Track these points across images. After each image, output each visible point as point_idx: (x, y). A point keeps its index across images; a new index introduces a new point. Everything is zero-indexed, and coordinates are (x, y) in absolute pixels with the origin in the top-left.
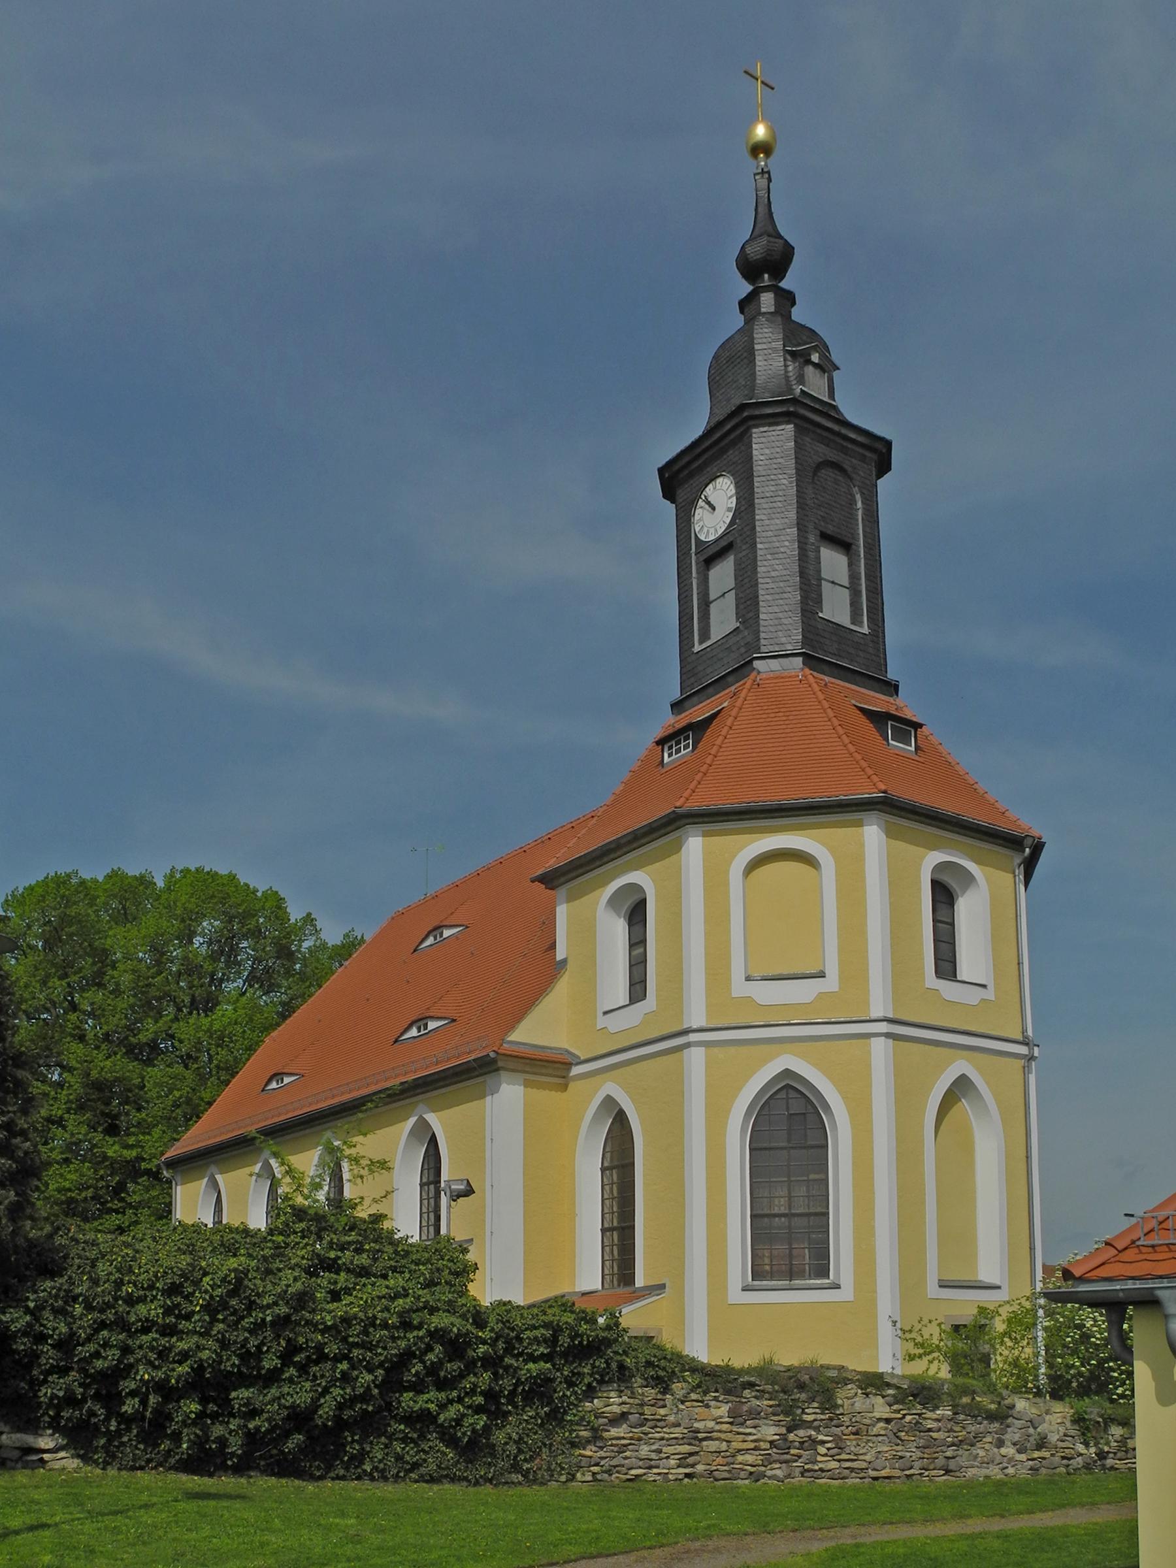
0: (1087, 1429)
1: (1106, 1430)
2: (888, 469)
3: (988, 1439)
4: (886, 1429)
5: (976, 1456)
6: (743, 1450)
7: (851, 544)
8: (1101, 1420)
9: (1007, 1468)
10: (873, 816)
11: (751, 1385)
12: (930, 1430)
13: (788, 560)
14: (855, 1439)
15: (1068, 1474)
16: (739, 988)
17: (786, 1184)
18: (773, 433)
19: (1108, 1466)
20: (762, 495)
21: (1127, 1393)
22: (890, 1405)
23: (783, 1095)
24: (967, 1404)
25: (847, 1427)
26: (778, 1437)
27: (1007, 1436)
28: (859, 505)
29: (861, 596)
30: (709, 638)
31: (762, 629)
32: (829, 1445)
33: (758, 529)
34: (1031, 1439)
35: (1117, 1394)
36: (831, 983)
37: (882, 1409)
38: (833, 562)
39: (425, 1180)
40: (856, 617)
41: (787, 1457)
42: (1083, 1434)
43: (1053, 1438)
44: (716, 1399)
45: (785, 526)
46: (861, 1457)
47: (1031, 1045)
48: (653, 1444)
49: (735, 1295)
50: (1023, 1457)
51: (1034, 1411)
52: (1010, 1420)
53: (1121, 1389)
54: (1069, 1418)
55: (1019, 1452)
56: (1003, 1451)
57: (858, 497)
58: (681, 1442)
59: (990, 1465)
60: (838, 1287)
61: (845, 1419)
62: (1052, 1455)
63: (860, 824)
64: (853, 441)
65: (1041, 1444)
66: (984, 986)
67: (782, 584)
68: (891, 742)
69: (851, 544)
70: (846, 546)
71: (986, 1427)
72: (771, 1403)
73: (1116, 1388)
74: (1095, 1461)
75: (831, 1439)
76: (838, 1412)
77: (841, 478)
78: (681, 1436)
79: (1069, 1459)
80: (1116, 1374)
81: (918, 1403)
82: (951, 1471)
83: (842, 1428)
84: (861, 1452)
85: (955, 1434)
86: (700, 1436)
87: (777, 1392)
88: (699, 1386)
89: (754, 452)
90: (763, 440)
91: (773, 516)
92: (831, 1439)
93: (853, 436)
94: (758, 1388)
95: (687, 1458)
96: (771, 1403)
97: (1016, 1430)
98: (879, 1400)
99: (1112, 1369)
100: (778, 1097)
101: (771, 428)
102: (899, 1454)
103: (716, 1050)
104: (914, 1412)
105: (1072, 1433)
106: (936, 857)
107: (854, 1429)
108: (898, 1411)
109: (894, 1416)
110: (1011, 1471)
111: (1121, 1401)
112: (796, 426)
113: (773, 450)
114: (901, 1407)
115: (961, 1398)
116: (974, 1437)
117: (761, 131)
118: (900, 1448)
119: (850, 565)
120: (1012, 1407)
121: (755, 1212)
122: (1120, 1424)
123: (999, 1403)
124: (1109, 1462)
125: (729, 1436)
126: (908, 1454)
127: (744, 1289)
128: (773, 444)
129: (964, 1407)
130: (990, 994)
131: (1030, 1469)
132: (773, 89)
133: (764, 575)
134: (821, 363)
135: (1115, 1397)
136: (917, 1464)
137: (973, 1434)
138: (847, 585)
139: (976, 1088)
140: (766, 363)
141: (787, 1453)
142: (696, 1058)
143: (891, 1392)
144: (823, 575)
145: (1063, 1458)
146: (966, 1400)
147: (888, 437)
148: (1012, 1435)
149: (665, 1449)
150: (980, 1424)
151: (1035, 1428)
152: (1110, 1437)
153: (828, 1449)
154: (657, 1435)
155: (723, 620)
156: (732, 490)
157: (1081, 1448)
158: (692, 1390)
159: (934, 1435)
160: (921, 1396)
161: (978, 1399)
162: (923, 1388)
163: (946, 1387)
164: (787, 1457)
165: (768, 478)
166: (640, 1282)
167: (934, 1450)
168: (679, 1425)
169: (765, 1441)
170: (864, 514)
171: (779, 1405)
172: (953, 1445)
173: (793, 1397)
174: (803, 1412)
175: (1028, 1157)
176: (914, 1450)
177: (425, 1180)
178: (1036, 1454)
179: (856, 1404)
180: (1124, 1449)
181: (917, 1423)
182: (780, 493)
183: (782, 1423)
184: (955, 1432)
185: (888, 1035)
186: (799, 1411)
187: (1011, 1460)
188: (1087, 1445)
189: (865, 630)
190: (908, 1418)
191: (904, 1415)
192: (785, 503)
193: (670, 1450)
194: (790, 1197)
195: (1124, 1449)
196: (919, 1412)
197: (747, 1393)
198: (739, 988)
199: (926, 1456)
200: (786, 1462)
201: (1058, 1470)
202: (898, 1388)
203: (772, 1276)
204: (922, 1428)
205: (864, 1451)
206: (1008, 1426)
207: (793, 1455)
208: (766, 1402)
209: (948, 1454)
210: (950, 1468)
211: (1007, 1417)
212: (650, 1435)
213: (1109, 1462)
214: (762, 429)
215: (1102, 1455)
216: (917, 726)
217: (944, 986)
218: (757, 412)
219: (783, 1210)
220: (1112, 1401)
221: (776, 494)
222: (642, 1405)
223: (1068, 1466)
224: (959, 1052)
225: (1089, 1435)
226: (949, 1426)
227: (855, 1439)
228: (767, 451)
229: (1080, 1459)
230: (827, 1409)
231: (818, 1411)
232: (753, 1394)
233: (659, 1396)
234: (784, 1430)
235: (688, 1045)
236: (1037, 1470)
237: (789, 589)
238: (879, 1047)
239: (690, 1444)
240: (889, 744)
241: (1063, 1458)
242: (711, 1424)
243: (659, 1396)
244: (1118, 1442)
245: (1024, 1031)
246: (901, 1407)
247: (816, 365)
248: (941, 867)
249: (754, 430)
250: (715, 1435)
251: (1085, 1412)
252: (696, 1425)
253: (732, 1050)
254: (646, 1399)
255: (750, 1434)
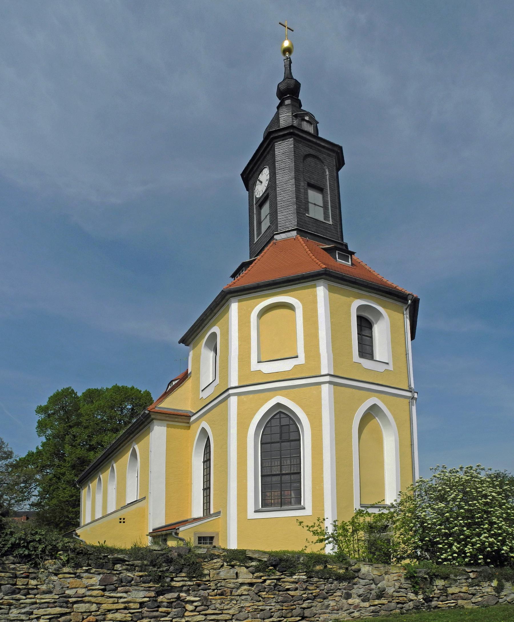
0: (416, 583)
1: (431, 583)
2: (343, 164)
3: (339, 593)
4: (249, 590)
5: (328, 606)
6: (113, 610)
7: (324, 189)
8: (427, 576)
9: (353, 612)
10: (322, 282)
11: (122, 561)
12: (288, 590)
13: (291, 193)
14: (220, 599)
15: (402, 613)
16: (255, 366)
17: (279, 459)
18: (284, 143)
19: (433, 606)
20: (279, 168)
21: (449, 557)
22: (253, 574)
23: (278, 416)
24: (321, 570)
25: (214, 590)
26: (147, 599)
27: (353, 591)
28: (327, 173)
29: (328, 210)
30: (261, 234)
31: (279, 223)
32: (195, 604)
33: (277, 182)
34: (373, 592)
35: (442, 559)
36: (301, 360)
37: (245, 576)
38: (314, 196)
39: (205, 487)
40: (326, 217)
41: (155, 614)
42: (414, 587)
43: (390, 591)
44: (87, 571)
45: (289, 179)
46: (225, 612)
47: (413, 392)
48: (24, 607)
49: (251, 514)
50: (367, 604)
51: (376, 572)
52: (356, 580)
53: (445, 555)
54: (403, 576)
55: (363, 601)
56: (350, 601)
57: (327, 170)
58: (52, 605)
59: (340, 611)
60: (304, 508)
61: (211, 584)
62: (389, 602)
63: (315, 286)
64: (324, 147)
65: (381, 595)
66: (387, 363)
67: (288, 203)
68: (338, 259)
69: (324, 189)
70: (320, 189)
71: (336, 586)
72: (141, 574)
73: (442, 555)
74: (423, 604)
75: (198, 599)
76: (204, 579)
77: (318, 162)
78: (53, 601)
79: (403, 604)
80: (441, 546)
81: (278, 571)
82: (307, 617)
83: (208, 591)
84: (225, 608)
85: (309, 592)
86: (71, 600)
87: (146, 565)
88: (68, 561)
89: (276, 152)
90: (280, 147)
91: (284, 176)
92: (198, 599)
93: (323, 144)
94: (127, 563)
95: (60, 617)
96: (141, 574)
97: (361, 587)
98: (244, 570)
99: (438, 543)
100: (275, 418)
101: (283, 142)
102: (260, 608)
103: (243, 397)
104: (272, 577)
105: (405, 586)
106: (358, 302)
107: (219, 591)
108: (257, 578)
109: (254, 581)
110: (356, 614)
111: (445, 563)
112: (294, 139)
113: (284, 150)
114: (261, 574)
115: (314, 566)
116: (327, 593)
117: (286, 44)
118: (261, 604)
119: (323, 197)
120: (359, 570)
121: (263, 474)
122: (442, 578)
123: (347, 569)
124: (434, 603)
125: (100, 599)
126: (268, 608)
127: (256, 512)
128: (284, 148)
129: (317, 572)
130: (391, 367)
131: (372, 612)
132: (293, 31)
133: (280, 200)
134: (310, 120)
135: (440, 560)
136: (276, 614)
137: (325, 591)
138: (322, 205)
139: (382, 411)
140: (284, 122)
141: (157, 611)
142: (233, 401)
143: (254, 563)
144: (310, 200)
145: (398, 603)
146: (318, 568)
147: (340, 145)
148: (359, 589)
149: (35, 612)
150: (332, 583)
151: (376, 584)
152: (435, 587)
153: (196, 607)
154: (28, 601)
155: (265, 225)
156: (268, 171)
157: (412, 596)
158: (64, 565)
159: (292, 593)
160: (279, 566)
161: (329, 566)
162: (281, 560)
163: (302, 559)
164: (155, 614)
165: (282, 161)
166: (212, 512)
167: (292, 603)
168: (50, 592)
169: (135, 602)
170: (329, 176)
171: (149, 575)
172: (308, 599)
173: (161, 569)
174: (172, 580)
175: (412, 445)
176: (273, 604)
177: (205, 487)
178: (377, 602)
179: (221, 573)
180: (445, 594)
181: (276, 585)
182: (287, 166)
183: (152, 589)
184: (310, 590)
185: (330, 383)
186: (168, 580)
187: (356, 607)
188: (416, 594)
189: (331, 223)
190: (268, 582)
191: (265, 581)
192: (289, 170)
193: (41, 612)
194: (281, 466)
195: (445, 594)
196: (277, 577)
197: (118, 566)
198: (255, 366)
199: (284, 608)
200: (155, 617)
201: (394, 612)
202: (260, 561)
203: (271, 505)
204: (281, 589)
205: (228, 607)
206: (355, 584)
207: (161, 612)
208: (137, 574)
209: (304, 606)
210: (305, 615)
211: (354, 578)
212: (21, 601)
213: (434, 603)
214: (279, 143)
215: (428, 600)
216: (352, 253)
217: (366, 363)
218: (276, 135)
219: (278, 472)
220: (438, 563)
221: (285, 167)
222: (16, 577)
223: (402, 608)
224: (373, 393)
225: (417, 587)
226: (304, 587)
227: (220, 599)
228: (282, 151)
229: (411, 603)
230: (194, 577)
231: (186, 579)
232: (124, 567)
233: (31, 570)
234: (153, 594)
235: (229, 396)
236: (378, 612)
237: (291, 204)
238: (325, 389)
239: (61, 607)
240: (337, 261)
241: (398, 603)
242: (81, 591)
243: (31, 570)
244: (440, 590)
245: (409, 385)
246: (261, 574)
247: (308, 121)
248: (360, 308)
249: (275, 144)
250: (86, 599)
251: (416, 573)
252: (68, 592)
253: (251, 396)
254: (18, 573)
255: (121, 598)
